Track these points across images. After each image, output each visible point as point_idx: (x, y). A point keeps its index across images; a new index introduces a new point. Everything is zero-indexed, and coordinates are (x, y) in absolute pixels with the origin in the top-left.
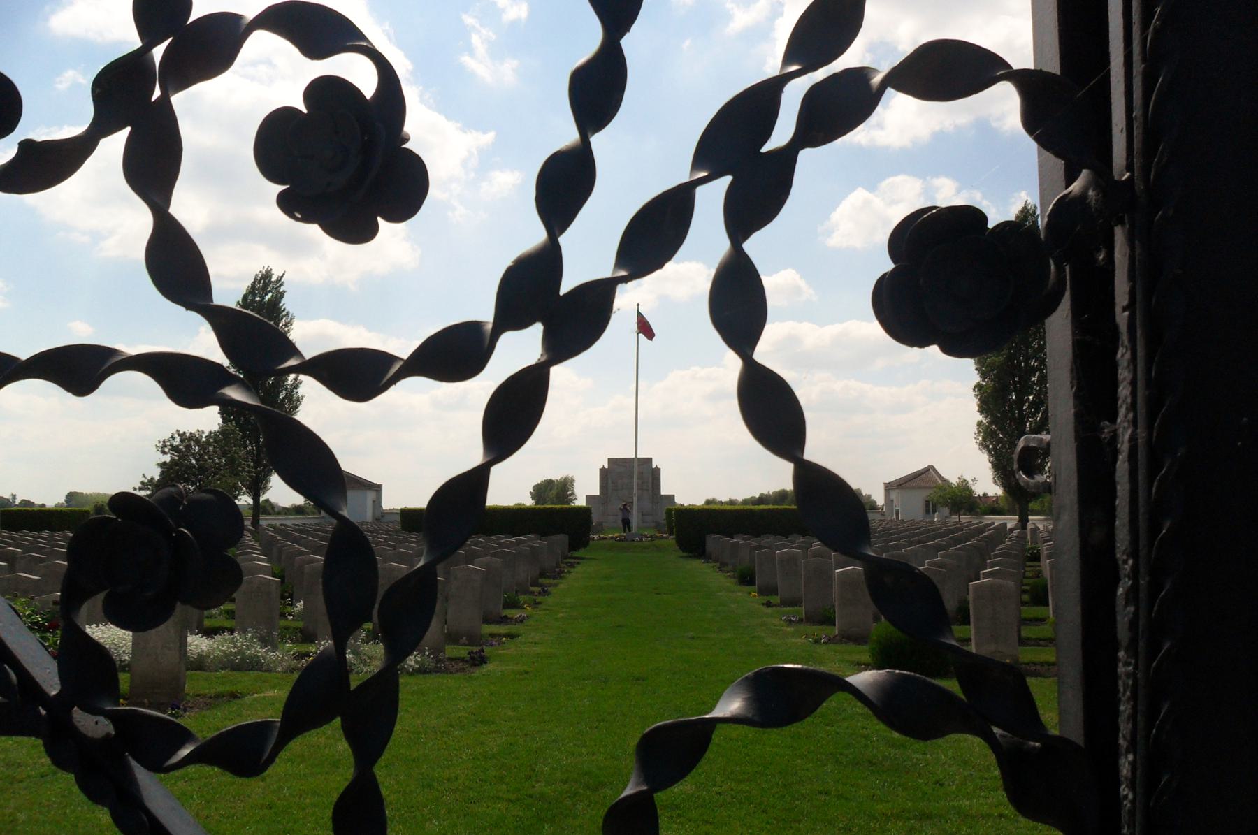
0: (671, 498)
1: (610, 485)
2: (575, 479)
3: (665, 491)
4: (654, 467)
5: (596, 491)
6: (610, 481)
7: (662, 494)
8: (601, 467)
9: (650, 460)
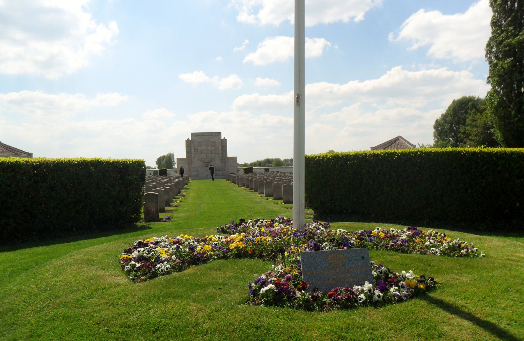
0: (234, 159)
1: (193, 151)
2: (175, 154)
3: (230, 154)
4: (222, 138)
5: (183, 155)
6: (193, 148)
7: (228, 156)
8: (187, 139)
9: (220, 134)
